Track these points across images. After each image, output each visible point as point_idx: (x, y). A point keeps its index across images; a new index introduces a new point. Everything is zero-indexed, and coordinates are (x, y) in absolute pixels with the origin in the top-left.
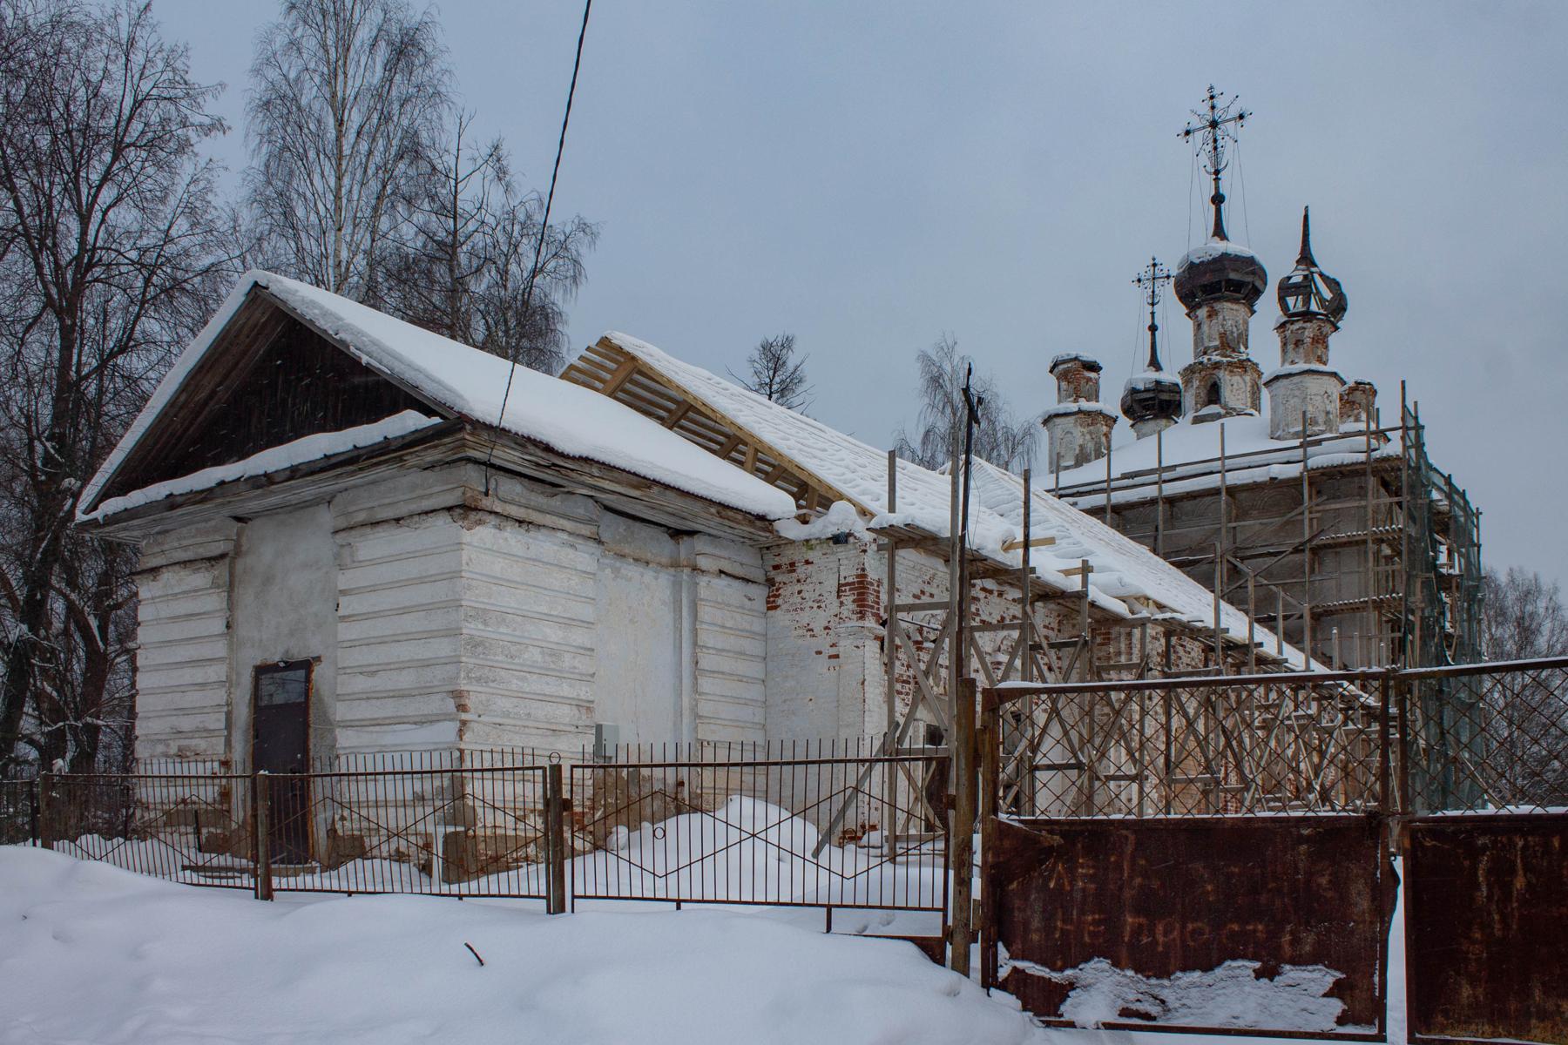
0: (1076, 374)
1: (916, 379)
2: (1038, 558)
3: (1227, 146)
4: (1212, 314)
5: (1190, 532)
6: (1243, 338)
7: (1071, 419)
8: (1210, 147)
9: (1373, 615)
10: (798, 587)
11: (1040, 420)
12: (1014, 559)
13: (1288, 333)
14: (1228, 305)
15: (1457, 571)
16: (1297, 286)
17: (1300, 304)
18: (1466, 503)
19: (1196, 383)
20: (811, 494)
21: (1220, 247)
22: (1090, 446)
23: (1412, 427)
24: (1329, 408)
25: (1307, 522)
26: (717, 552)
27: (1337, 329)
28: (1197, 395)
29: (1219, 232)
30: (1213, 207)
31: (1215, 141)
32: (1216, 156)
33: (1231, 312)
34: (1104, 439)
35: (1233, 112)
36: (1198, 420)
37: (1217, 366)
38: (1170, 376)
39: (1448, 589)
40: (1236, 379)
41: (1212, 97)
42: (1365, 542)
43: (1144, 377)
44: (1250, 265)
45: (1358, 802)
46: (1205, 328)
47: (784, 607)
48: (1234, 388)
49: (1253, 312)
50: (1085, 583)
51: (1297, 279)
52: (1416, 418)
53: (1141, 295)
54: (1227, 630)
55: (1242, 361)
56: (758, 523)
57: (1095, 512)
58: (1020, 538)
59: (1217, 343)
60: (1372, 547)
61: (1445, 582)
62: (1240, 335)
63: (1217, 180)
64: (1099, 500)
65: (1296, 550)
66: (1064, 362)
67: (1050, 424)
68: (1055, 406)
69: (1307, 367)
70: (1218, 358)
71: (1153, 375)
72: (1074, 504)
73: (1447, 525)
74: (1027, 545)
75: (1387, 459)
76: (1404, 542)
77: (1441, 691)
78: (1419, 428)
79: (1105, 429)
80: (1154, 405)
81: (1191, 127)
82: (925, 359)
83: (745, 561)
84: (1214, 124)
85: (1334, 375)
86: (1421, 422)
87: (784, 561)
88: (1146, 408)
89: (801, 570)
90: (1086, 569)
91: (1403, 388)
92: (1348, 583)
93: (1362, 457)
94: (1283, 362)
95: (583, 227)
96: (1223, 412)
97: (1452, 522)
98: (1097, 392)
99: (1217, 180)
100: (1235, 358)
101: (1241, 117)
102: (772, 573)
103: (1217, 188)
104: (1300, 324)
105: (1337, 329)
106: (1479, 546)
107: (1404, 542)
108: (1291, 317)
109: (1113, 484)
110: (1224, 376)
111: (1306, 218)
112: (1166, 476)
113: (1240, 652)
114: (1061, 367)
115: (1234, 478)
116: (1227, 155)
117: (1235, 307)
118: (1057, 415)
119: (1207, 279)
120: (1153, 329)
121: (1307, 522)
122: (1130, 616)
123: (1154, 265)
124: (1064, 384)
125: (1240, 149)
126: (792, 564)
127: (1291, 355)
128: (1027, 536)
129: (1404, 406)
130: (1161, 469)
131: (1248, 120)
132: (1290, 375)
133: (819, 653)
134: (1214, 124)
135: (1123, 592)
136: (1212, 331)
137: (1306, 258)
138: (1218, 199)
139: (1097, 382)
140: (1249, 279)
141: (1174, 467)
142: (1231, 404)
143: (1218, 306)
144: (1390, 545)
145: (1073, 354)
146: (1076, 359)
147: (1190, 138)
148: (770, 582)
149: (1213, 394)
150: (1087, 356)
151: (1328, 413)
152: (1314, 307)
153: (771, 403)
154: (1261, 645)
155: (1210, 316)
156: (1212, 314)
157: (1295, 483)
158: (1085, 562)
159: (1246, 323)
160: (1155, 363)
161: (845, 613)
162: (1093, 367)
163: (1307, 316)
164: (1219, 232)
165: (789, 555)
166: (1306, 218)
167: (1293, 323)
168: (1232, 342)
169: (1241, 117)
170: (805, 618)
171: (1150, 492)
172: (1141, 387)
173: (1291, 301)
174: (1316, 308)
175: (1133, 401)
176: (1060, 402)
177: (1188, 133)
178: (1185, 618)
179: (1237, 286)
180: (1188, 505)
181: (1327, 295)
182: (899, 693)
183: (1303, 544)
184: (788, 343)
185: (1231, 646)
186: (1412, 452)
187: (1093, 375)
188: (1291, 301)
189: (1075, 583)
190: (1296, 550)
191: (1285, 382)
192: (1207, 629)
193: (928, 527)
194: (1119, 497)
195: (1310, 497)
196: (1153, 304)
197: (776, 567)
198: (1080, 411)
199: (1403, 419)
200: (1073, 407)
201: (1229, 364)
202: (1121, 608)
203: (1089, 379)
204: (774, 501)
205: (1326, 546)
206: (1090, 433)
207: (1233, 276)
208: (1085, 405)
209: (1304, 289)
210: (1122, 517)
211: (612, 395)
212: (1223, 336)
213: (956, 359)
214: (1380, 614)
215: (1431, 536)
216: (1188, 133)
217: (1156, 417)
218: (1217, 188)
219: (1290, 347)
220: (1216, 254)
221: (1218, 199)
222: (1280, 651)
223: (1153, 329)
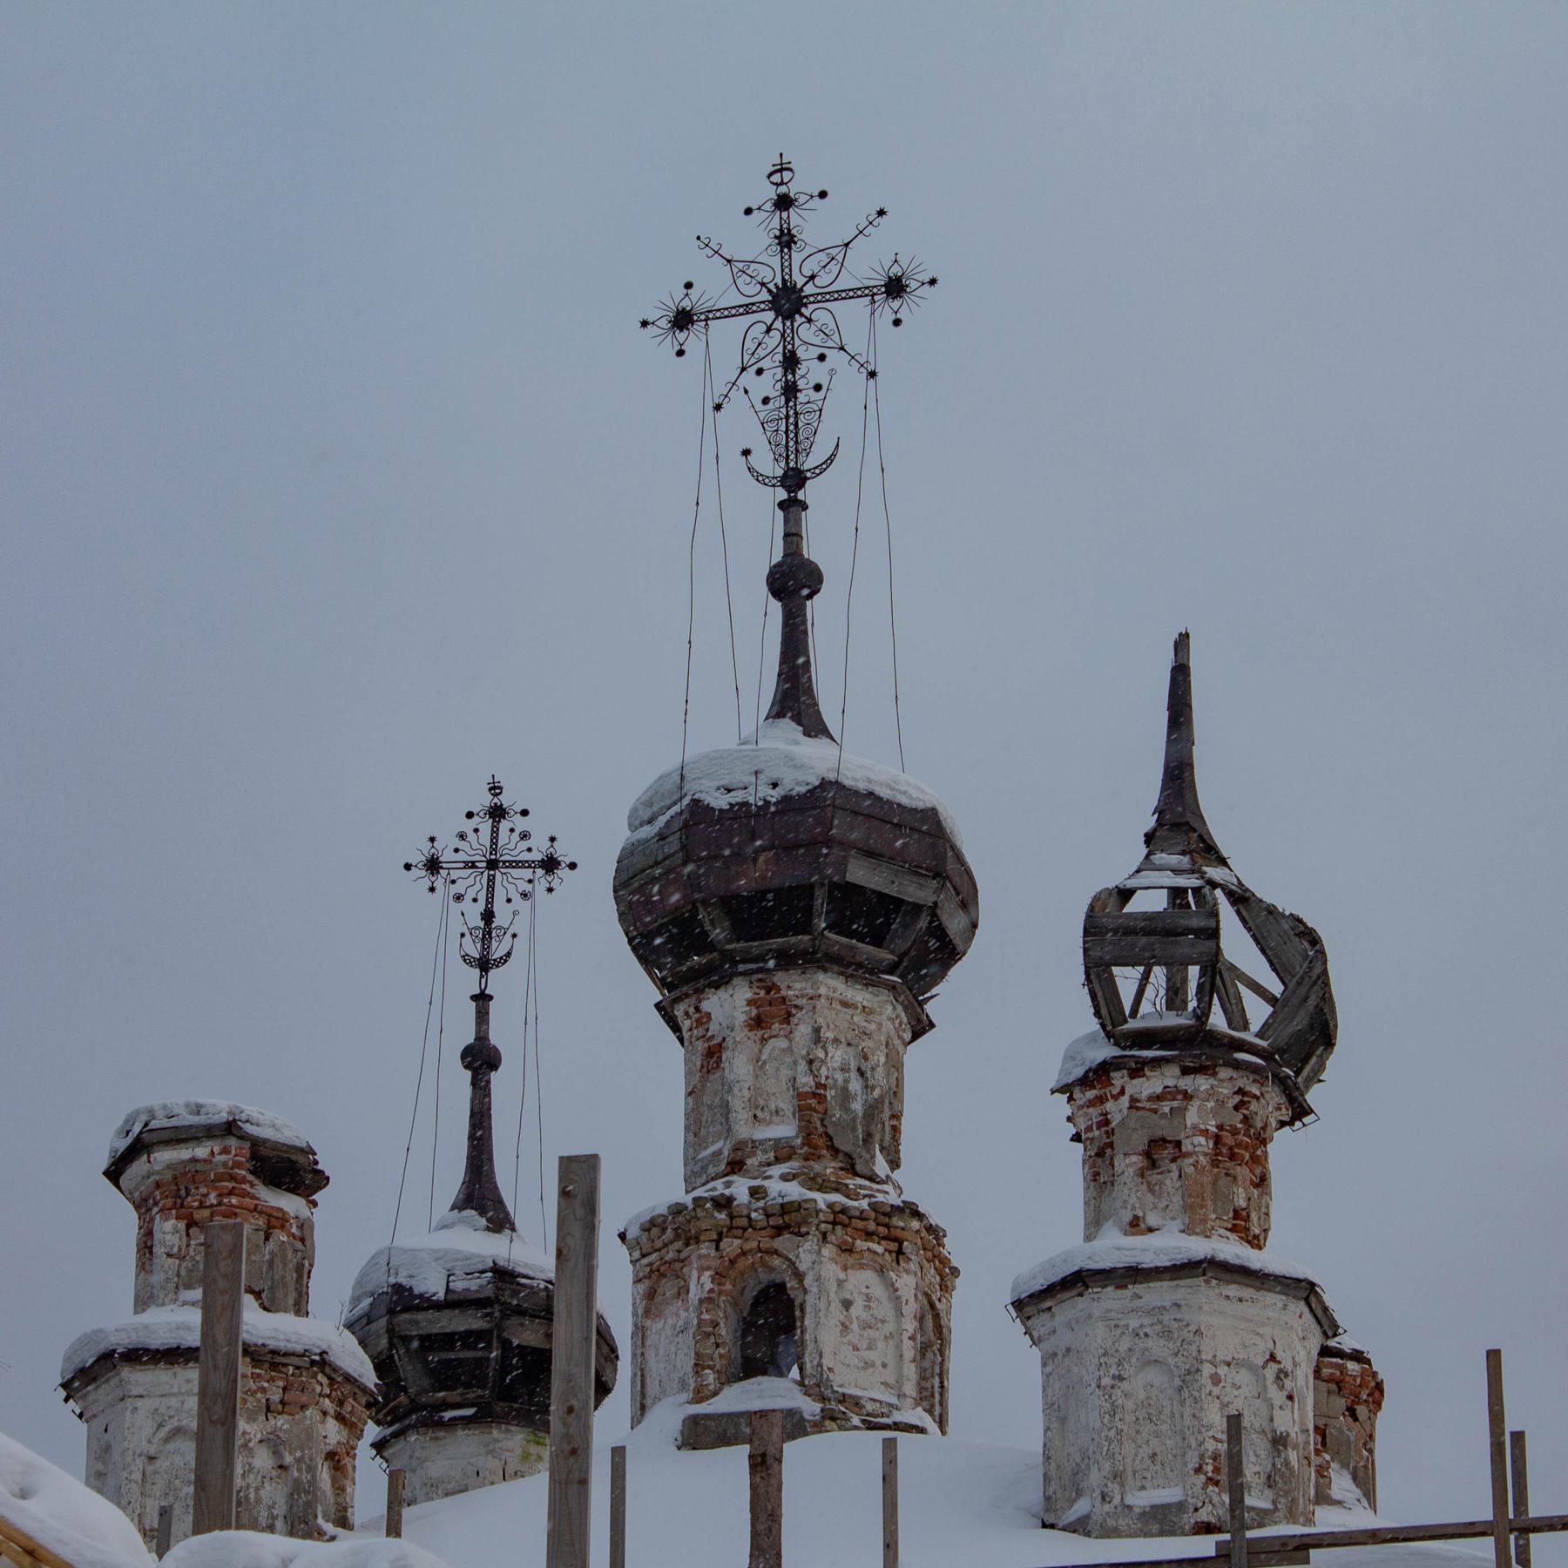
4: (769, 1016)
6: (882, 1123)
8: (770, 384)
13: (1117, 1110)
14: (830, 984)
16: (1151, 926)
17: (1175, 997)
19: (700, 1283)
21: (801, 761)
27: (1300, 1111)
28: (706, 1331)
29: (795, 699)
30: (776, 607)
31: (791, 362)
32: (792, 420)
34: (324, 1476)
35: (865, 267)
37: (789, 1219)
40: (863, 1280)
41: (784, 203)
46: (738, 1066)
49: (921, 1026)
51: (1149, 902)
53: (437, 922)
55: (884, 1213)
59: (785, 1129)
63: (792, 507)
66: (180, 1136)
67: (102, 1393)
68: (117, 1317)
69: (1198, 1247)
70: (794, 1191)
71: (476, 1244)
81: (697, 300)
84: (788, 302)
85: (1306, 1291)
88: (445, 1377)
94: (1094, 1223)
96: (810, 1408)
98: (302, 1273)
99: (792, 507)
101: (895, 288)
103: (792, 537)
104: (1169, 1077)
105: (1300, 1111)
108: (1131, 1046)
110: (817, 1264)
111: (1180, 674)
114: (165, 1157)
116: (838, 417)
117: (859, 995)
118: (136, 1356)
119: (759, 872)
120: (481, 1059)
123: (497, 813)
124: (168, 1230)
125: (887, 406)
127: (1129, 1193)
131: (918, 307)
132: (1134, 1274)
134: (788, 302)
136: (765, 1079)
137: (1178, 823)
138: (793, 581)
139: (304, 1236)
140: (915, 891)
142: (845, 1380)
143: (793, 985)
145: (219, 1107)
146: (230, 1128)
147: (692, 339)
149: (768, 1326)
150: (278, 1121)
155: (758, 1023)
156: (769, 1016)
159: (895, 1064)
160: (481, 1196)
162: (293, 1170)
163: (1197, 1048)
164: (795, 699)
166: (1180, 674)
168: (846, 1135)
169: (895, 288)
172: (432, 1284)
173: (1126, 979)
174: (1212, 1024)
176: (143, 1301)
177: (682, 320)
179: (868, 915)
187: (290, 1204)
188: (1126, 979)
191: (1110, 1298)
200: (179, 1321)
201: (840, 1217)
203: (276, 1220)
207: (860, 873)
209: (1180, 936)
212: (810, 1104)
216: (682, 320)
217: (485, 1417)
218: (792, 537)
219: (1127, 1164)
220: (796, 782)
221: (793, 581)
223: (481, 1059)
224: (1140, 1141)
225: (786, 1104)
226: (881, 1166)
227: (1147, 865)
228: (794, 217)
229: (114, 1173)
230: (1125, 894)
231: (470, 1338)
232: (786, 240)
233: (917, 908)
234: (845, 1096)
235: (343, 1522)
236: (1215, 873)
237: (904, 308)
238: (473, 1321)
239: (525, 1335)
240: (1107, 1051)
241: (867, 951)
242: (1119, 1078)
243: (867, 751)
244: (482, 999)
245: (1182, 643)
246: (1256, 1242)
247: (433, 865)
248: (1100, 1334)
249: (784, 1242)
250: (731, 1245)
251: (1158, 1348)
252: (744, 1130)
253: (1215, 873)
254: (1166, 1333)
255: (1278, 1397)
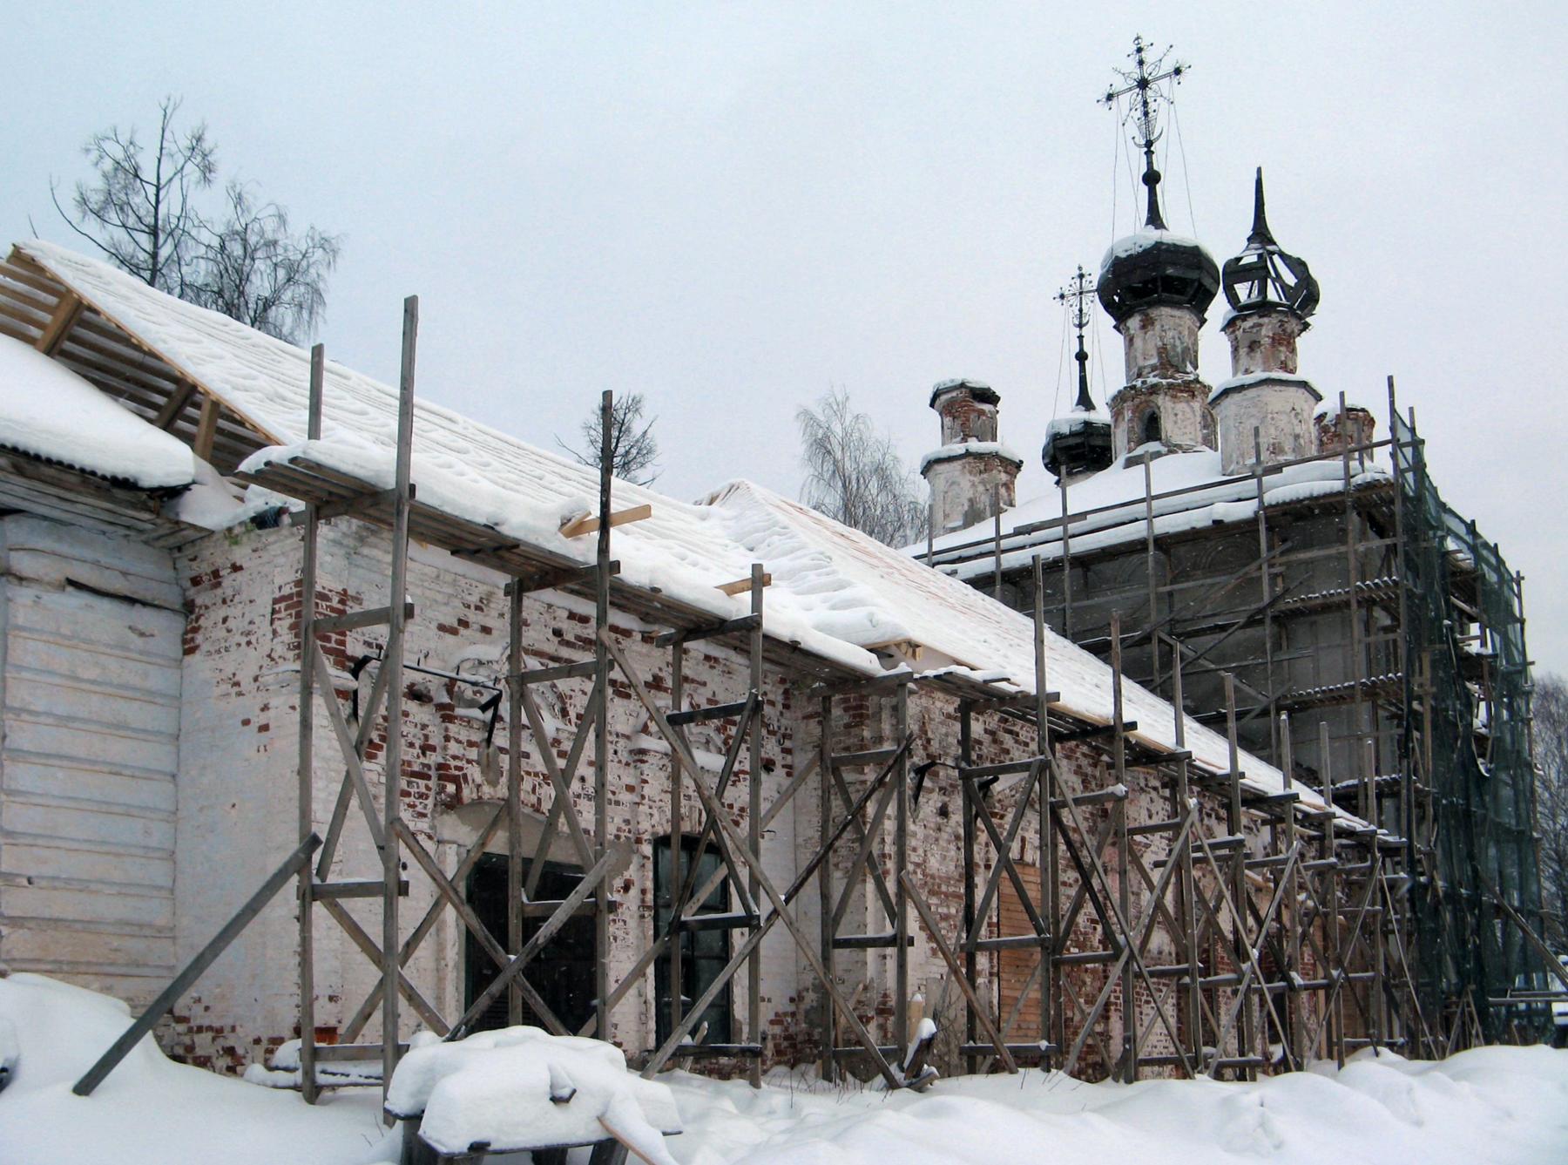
0: (967, 405)
1: (798, 446)
2: (621, 544)
3: (1158, 106)
4: (1147, 324)
5: (1114, 603)
7: (957, 465)
8: (1139, 114)
9: (1363, 711)
10: (223, 611)
11: (918, 466)
12: (583, 551)
13: (1239, 333)
15: (1489, 650)
18: (1501, 561)
19: (1128, 415)
20: (227, 441)
22: (984, 501)
23: (1409, 444)
24: (1298, 430)
25: (1266, 580)
26: (64, 549)
28: (1130, 430)
29: (1154, 218)
31: (1145, 103)
32: (1147, 123)
33: (1171, 320)
35: (1168, 67)
36: (1131, 463)
37: (1154, 390)
38: (1102, 415)
39: (1479, 679)
40: (1181, 407)
41: (1139, 50)
42: (1347, 604)
43: (1069, 416)
44: (1194, 257)
45: (1335, 973)
46: (1138, 342)
47: (205, 647)
48: (1178, 418)
50: (757, 603)
51: (1250, 258)
52: (1413, 430)
53: (1065, 314)
54: (1057, 696)
55: (1187, 384)
56: (119, 493)
57: (981, 583)
58: (596, 512)
59: (1154, 361)
60: (1357, 614)
61: (1473, 666)
62: (1186, 350)
63: (1149, 153)
64: (986, 565)
65: (1252, 622)
67: (931, 474)
72: (953, 573)
73: (1474, 590)
74: (605, 522)
75: (1372, 486)
76: (1402, 601)
77: (1468, 814)
78: (1417, 444)
79: (1004, 477)
80: (1078, 452)
81: (1115, 89)
82: (808, 418)
83: (142, 568)
84: (1143, 84)
85: (1304, 385)
86: (1420, 434)
87: (203, 568)
89: (229, 581)
90: (759, 580)
91: (1391, 385)
92: (1330, 663)
93: (1338, 485)
94: (1235, 374)
95: (324, 244)
97: (1483, 588)
99: (1149, 153)
100: (1180, 378)
101: (1178, 71)
102: (192, 592)
103: (1150, 163)
105: (1306, 326)
106: (1522, 622)
107: (1402, 601)
109: (1004, 543)
110: (1164, 403)
111: (1259, 183)
112: (1073, 527)
113: (1104, 740)
114: (944, 398)
115: (1164, 525)
116: (1160, 123)
118: (939, 461)
121: (1266, 580)
122: (884, 673)
123: (1081, 276)
124: (948, 420)
125: (1177, 109)
126: (216, 574)
127: (1244, 361)
128: (605, 505)
129: (1393, 411)
130: (1066, 519)
131: (1186, 73)
133: (246, 722)
134: (1143, 84)
135: (875, 637)
136: (1148, 346)
137: (1260, 233)
138: (1151, 178)
140: (1193, 275)
141: (1082, 516)
142: (1176, 440)
144: (1386, 609)
146: (963, 385)
147: (1114, 103)
148: (189, 608)
149: (1151, 428)
150: (979, 380)
151: (1297, 437)
152: (1272, 295)
153: (184, 304)
154: (1133, 725)
155: (1144, 327)
156: (1147, 324)
157: (1246, 528)
158: (757, 568)
160: (1085, 401)
161: (280, 650)
164: (1154, 218)
165: (215, 556)
166: (1259, 183)
167: (1244, 318)
169: (1178, 71)
170: (229, 663)
171: (1052, 551)
172: (1065, 430)
174: (1280, 301)
175: (1054, 447)
177: (1110, 97)
178: (977, 676)
180: (1108, 568)
181: (1291, 280)
182: (407, 794)
183: (1261, 611)
184: (635, 405)
185: (1084, 730)
186: (1410, 476)
187: (987, 407)
189: (741, 606)
190: (1252, 622)
191: (1236, 397)
192: (1026, 696)
193: (345, 467)
194: (1011, 560)
195: (1270, 548)
196: (1080, 326)
197: (196, 581)
198: (968, 454)
199: (1393, 429)
200: (958, 448)
201: (1170, 386)
202: (869, 663)
203: (982, 412)
204: (155, 454)
205: (1295, 614)
206: (983, 482)
208: (974, 445)
209: (1258, 273)
210: (1012, 587)
211: (53, 350)
212: (1162, 351)
213: (848, 419)
214: (1375, 707)
215: (1447, 601)
216: (1110, 97)
218: (1150, 163)
219: (1243, 351)
222: (1180, 740)
223: (1082, 357)
224: (1247, 343)
225: (1154, 352)
226: (1189, 368)
227: (1247, 248)
228: (1143, 54)
229: (932, 405)
230: (1239, 259)
231: (1077, 446)
232: (1141, 63)
233: (1193, 281)
234: (1174, 346)
235: (1012, 505)
236: (1271, 248)
237: (1181, 78)
238: (1078, 440)
239: (1099, 442)
240: (1235, 313)
241: (1177, 297)
242: (1238, 323)
243: (1178, 230)
244: (1081, 337)
245: (1259, 170)
246: (1292, 372)
247: (1062, 297)
248: (1233, 407)
249: (1153, 398)
250: (1137, 401)
251: (1253, 411)
252: (1141, 363)
253: (1271, 248)
254: (1255, 406)
255: (1296, 422)
